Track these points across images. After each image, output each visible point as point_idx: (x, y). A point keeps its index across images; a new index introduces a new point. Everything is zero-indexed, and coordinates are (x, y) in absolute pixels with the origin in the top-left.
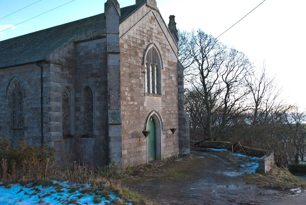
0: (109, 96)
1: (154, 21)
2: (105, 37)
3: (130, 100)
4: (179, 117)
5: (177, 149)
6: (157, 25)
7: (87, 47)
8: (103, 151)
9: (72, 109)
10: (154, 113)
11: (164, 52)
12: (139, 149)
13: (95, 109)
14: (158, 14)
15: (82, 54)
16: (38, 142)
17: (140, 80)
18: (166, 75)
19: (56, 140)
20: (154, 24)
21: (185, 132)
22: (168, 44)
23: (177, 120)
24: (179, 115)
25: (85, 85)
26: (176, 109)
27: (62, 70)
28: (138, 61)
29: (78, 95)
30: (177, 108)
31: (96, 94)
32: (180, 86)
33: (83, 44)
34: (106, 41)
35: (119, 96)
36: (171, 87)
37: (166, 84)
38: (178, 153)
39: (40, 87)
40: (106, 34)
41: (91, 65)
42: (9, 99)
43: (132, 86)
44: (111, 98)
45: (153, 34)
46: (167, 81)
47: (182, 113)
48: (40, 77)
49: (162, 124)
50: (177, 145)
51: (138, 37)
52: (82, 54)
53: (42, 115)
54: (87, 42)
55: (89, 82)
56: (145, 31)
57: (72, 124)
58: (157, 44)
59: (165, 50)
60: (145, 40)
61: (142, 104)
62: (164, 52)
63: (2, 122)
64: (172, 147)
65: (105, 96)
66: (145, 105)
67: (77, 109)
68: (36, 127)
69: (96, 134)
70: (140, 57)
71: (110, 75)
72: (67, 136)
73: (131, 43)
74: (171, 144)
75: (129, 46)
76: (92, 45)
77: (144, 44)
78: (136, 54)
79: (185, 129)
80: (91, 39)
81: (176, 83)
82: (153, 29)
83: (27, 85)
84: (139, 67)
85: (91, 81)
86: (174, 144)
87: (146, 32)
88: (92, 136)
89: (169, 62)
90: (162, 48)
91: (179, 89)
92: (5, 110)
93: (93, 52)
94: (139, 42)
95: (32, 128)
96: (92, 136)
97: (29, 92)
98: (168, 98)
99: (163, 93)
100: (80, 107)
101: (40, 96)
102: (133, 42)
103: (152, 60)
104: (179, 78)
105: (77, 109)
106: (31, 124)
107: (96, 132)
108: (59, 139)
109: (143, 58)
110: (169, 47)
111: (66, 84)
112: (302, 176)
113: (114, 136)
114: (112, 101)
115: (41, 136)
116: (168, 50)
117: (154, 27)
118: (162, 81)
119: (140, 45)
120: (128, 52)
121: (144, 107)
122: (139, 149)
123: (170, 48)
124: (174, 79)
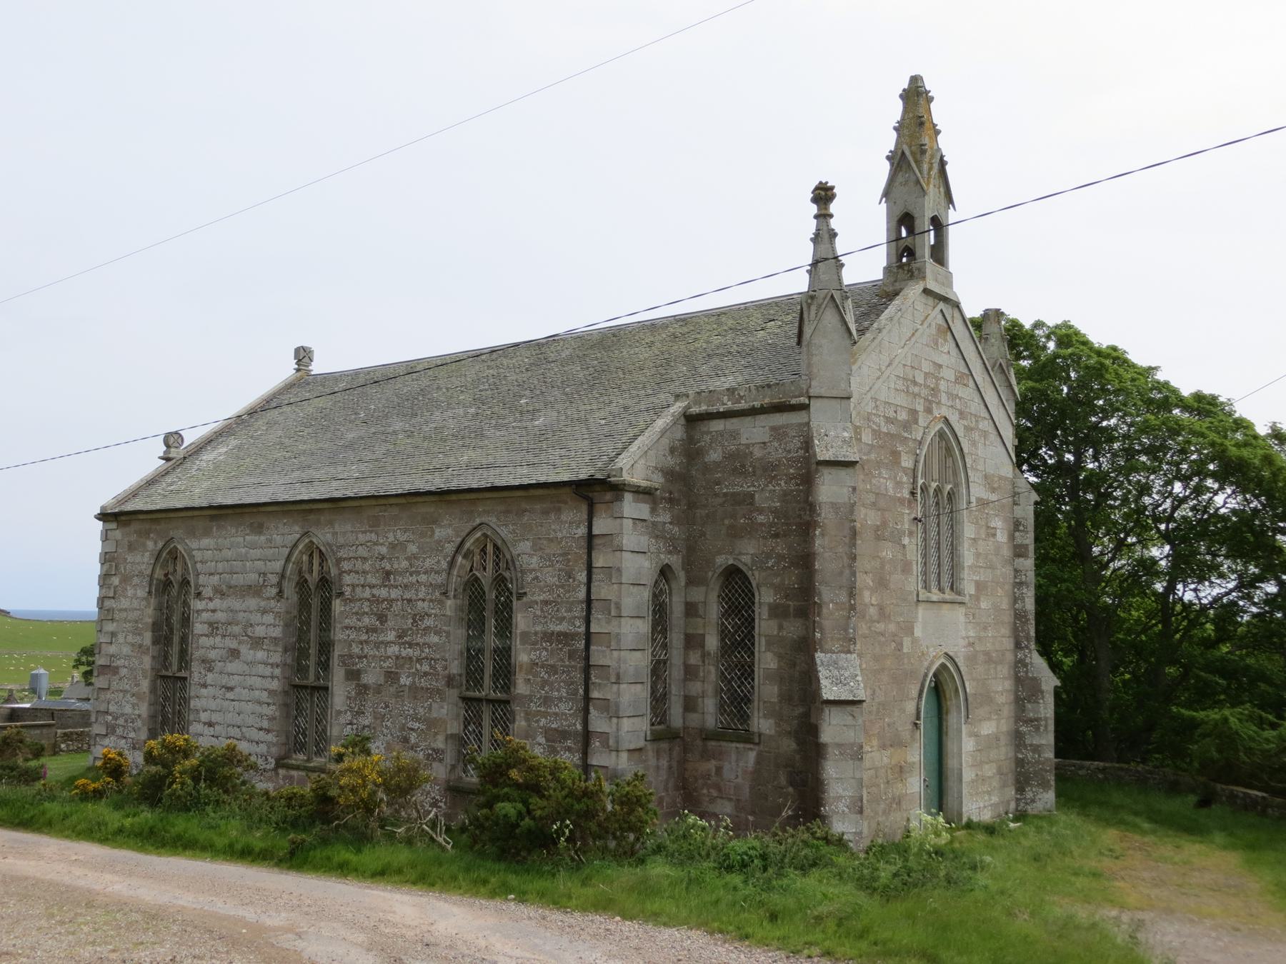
0: (820, 606)
1: (946, 340)
2: (805, 407)
3: (876, 618)
4: (1016, 674)
5: (1011, 792)
6: (954, 351)
7: (734, 435)
8: (791, 789)
9: (676, 639)
10: (942, 660)
11: (974, 444)
12: (898, 789)
13: (760, 645)
14: (957, 314)
15: (714, 456)
16: (569, 749)
17: (904, 546)
18: (977, 523)
19: (632, 747)
20: (945, 349)
21: (1037, 729)
22: (984, 414)
23: (1009, 684)
24: (1016, 666)
25: (722, 561)
26: (1009, 644)
27: (653, 511)
28: (899, 484)
29: (697, 594)
30: (1012, 640)
31: (765, 597)
32: (1021, 560)
33: (717, 426)
34: (806, 420)
35: (853, 608)
36: (992, 567)
37: (978, 555)
38: (1013, 805)
39: (584, 567)
40: (810, 398)
41: (752, 496)
42: (455, 597)
43: (882, 567)
44: (825, 611)
45: (943, 386)
46: (982, 547)
47: (1028, 660)
48: (582, 531)
49: (966, 700)
50: (1011, 779)
51: (901, 400)
52: (714, 456)
53: (582, 655)
54: (734, 420)
55: (740, 554)
56: (920, 379)
57: (674, 690)
58: (954, 419)
59: (976, 435)
60: (920, 408)
61: (910, 631)
62: (974, 444)
63: (426, 674)
64: (995, 783)
65: (803, 601)
66: (918, 632)
67: (693, 642)
68: (560, 699)
69: (763, 731)
70: (904, 470)
71: (822, 535)
72: (663, 735)
73: (883, 424)
74: (990, 774)
75: (877, 434)
76: (754, 432)
77: (916, 422)
78: (896, 455)
79: (1037, 720)
80: (752, 412)
81: (1006, 552)
82: (940, 366)
83: (531, 555)
84: (901, 501)
85: (747, 552)
86: (1000, 772)
87: (922, 382)
88: (748, 738)
89: (986, 477)
90: (968, 429)
91: (1016, 571)
92: (437, 633)
93: (758, 453)
94: (903, 416)
95: (547, 701)
96: (748, 738)
97: (537, 578)
98: (983, 605)
99: (969, 589)
100: (703, 635)
101: (582, 594)
102: (889, 420)
103: (936, 476)
104: (1017, 534)
105: (693, 642)
106: (542, 688)
107: (762, 724)
108: (641, 744)
109: (914, 470)
110: (986, 425)
111: (662, 556)
112: (493, 895)
113: (837, 740)
114: (827, 624)
115: (579, 727)
116: (985, 434)
117: (942, 359)
118: (966, 545)
119: (906, 426)
120: (873, 456)
121: (915, 641)
122: (898, 789)
123: (991, 429)
124: (1002, 537)
